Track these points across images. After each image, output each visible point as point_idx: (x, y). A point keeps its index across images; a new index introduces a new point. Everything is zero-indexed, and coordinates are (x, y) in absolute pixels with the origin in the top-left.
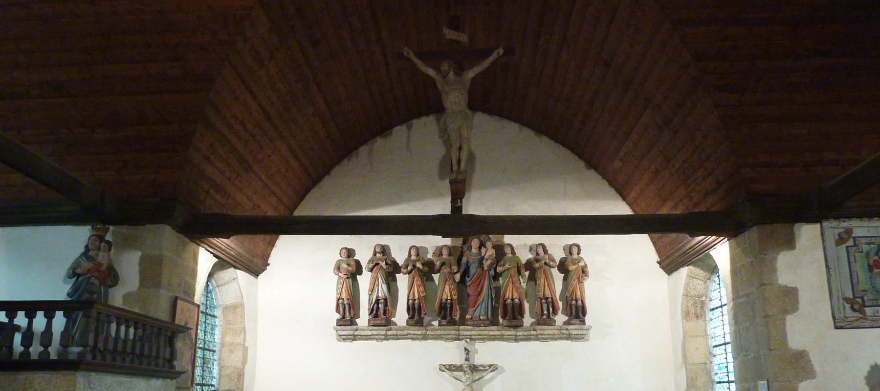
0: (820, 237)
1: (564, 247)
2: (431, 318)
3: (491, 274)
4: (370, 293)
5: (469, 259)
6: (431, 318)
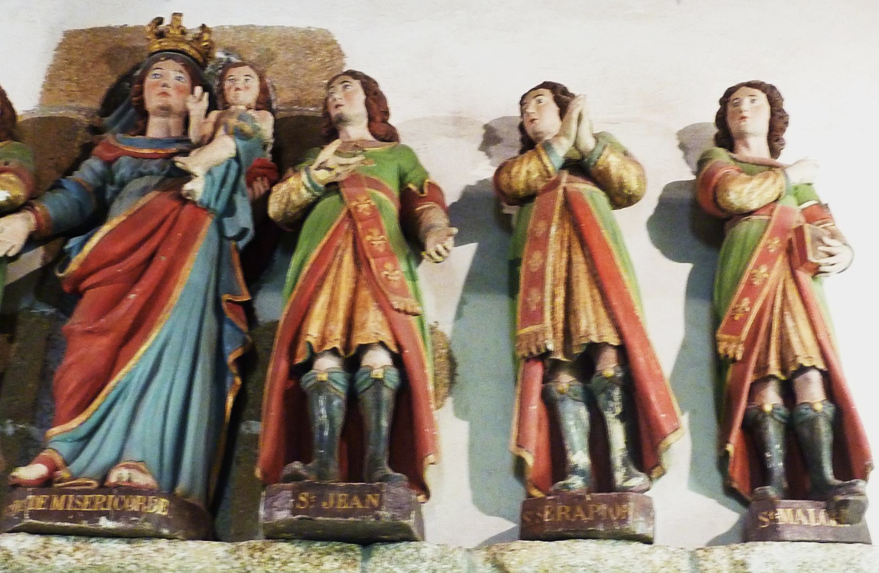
0: (853, 544)
1: (680, 134)
3: (231, 232)
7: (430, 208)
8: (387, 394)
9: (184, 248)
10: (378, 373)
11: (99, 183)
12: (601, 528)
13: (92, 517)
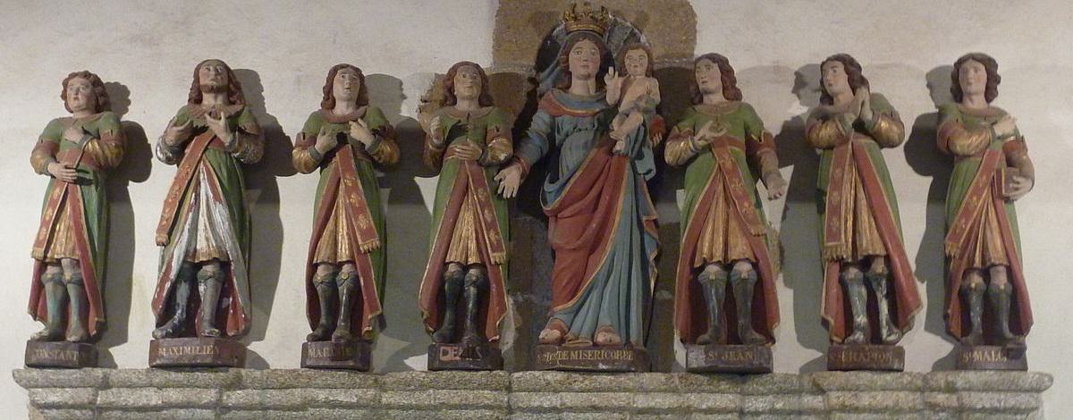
2: (404, 344)
4: (164, 238)
5: (559, 119)
6: (404, 344)
7: (768, 152)
8: (750, 287)
9: (616, 187)
10: (744, 275)
11: (549, 131)
12: (875, 366)
13: (595, 363)
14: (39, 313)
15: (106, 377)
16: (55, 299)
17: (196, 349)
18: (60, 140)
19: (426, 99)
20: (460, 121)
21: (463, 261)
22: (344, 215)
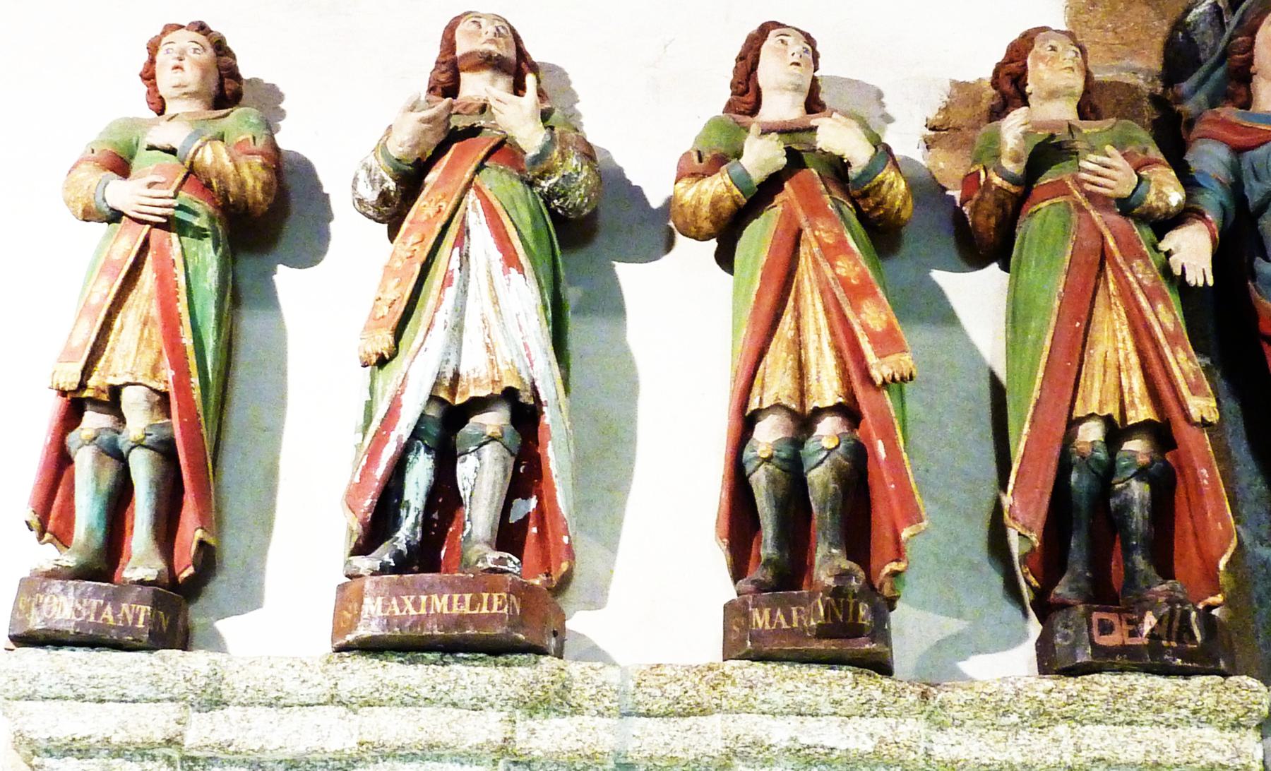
2: (954, 626)
4: (383, 342)
6: (954, 626)
14: (51, 524)
15: (215, 675)
16: (97, 491)
17: (461, 601)
18: (132, 157)
19: (937, 124)
20: (1052, 136)
21: (1112, 409)
22: (819, 307)
